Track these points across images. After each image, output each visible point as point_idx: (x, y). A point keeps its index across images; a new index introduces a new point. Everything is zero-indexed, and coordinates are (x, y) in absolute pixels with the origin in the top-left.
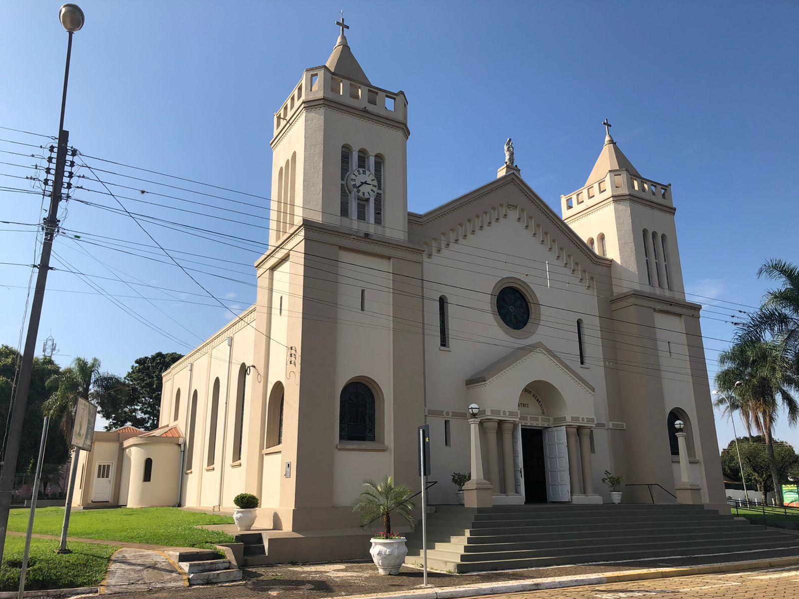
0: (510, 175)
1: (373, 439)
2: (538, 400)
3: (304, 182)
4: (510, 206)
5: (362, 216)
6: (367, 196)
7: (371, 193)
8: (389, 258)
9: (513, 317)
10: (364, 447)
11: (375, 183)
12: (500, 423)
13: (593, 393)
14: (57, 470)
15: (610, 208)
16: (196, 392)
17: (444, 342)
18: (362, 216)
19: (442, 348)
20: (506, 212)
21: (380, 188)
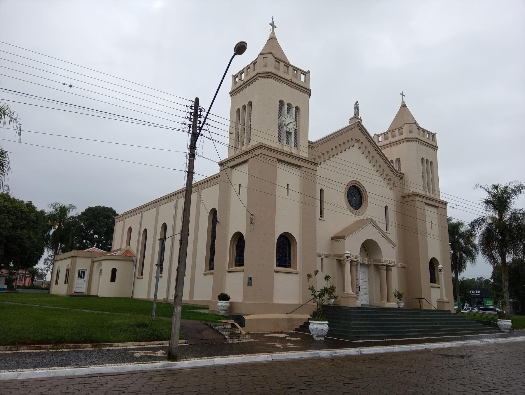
6: (291, 131)
7: (293, 129)
11: (295, 123)
14: (36, 271)
19: (321, 218)
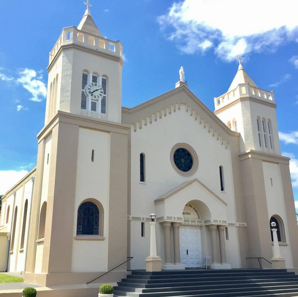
0: (182, 86)
1: (97, 233)
2: (196, 211)
3: (61, 90)
4: (181, 103)
5: (94, 108)
8: (109, 132)
9: (183, 165)
11: (102, 91)
12: (218, 226)
13: (226, 207)
15: (239, 105)
16: (17, 207)
17: (142, 179)
18: (94, 108)
19: (222, 191)
20: (180, 107)
21: (105, 93)
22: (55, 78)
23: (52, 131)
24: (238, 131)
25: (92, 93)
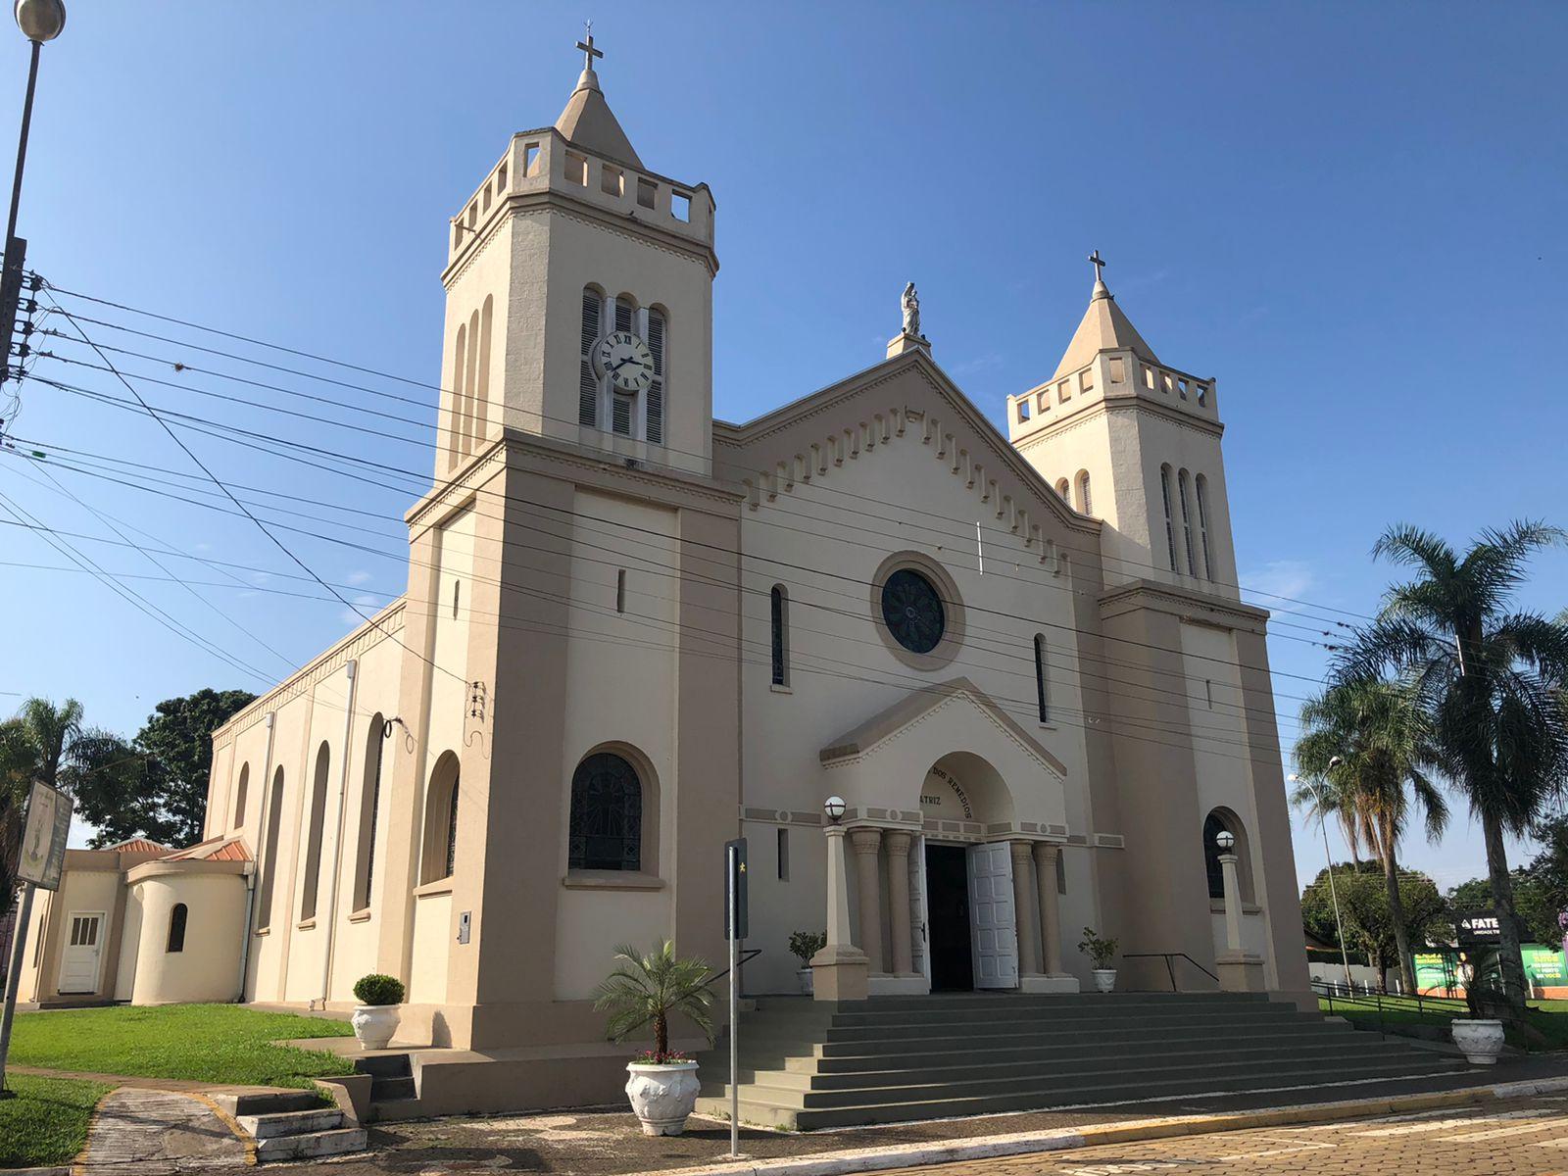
0: (911, 353)
1: (635, 866)
2: (958, 790)
5: (621, 425)
6: (632, 386)
7: (641, 380)
8: (675, 509)
9: (913, 629)
10: (619, 882)
11: (649, 360)
13: (1063, 778)
17: (779, 677)
18: (621, 425)
19: (777, 687)
21: (658, 372)
22: (477, 310)
23: (475, 499)
24: (1097, 514)
25: (618, 367)
